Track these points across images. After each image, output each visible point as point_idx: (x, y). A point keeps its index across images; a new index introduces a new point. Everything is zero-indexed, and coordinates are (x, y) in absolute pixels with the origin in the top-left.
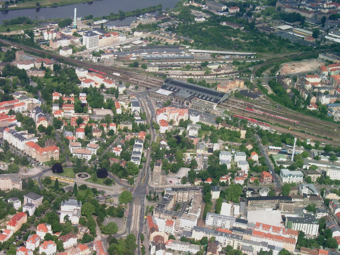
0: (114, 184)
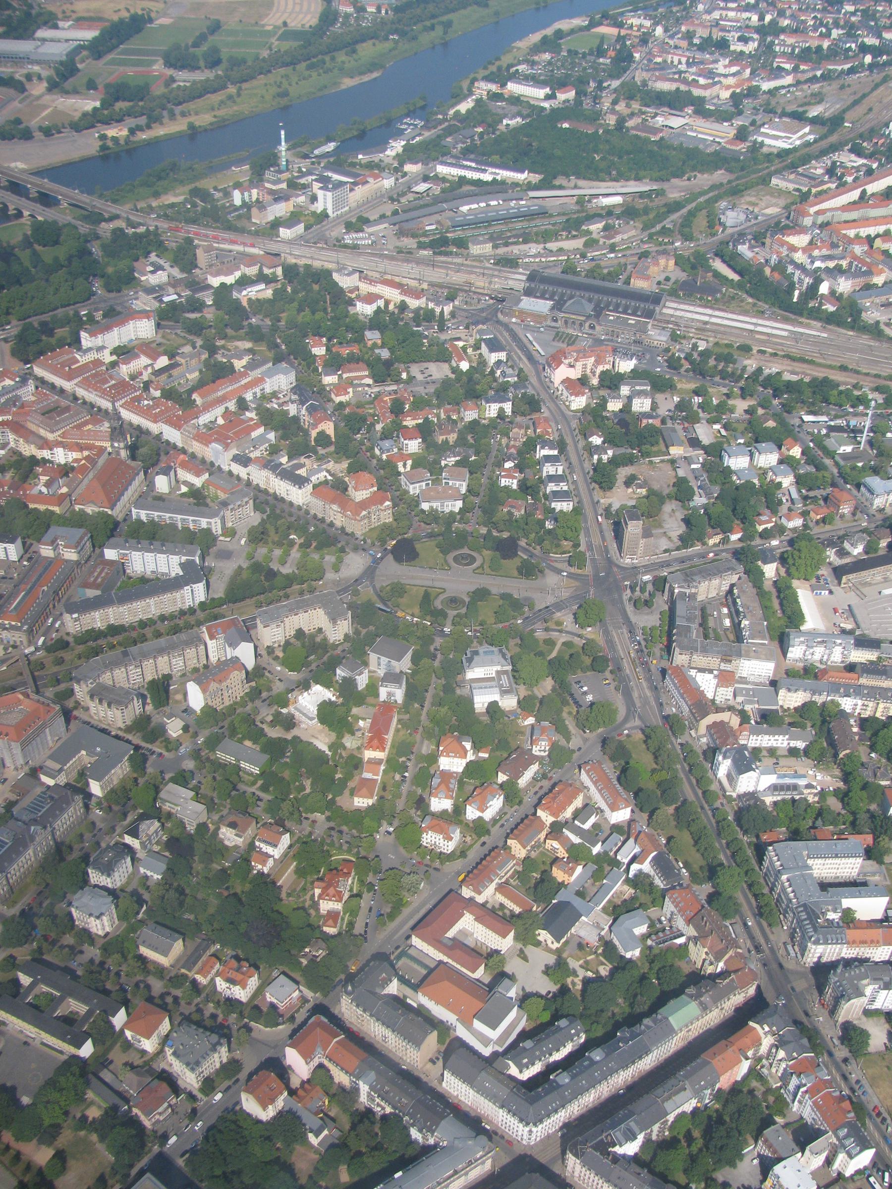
0: (541, 572)
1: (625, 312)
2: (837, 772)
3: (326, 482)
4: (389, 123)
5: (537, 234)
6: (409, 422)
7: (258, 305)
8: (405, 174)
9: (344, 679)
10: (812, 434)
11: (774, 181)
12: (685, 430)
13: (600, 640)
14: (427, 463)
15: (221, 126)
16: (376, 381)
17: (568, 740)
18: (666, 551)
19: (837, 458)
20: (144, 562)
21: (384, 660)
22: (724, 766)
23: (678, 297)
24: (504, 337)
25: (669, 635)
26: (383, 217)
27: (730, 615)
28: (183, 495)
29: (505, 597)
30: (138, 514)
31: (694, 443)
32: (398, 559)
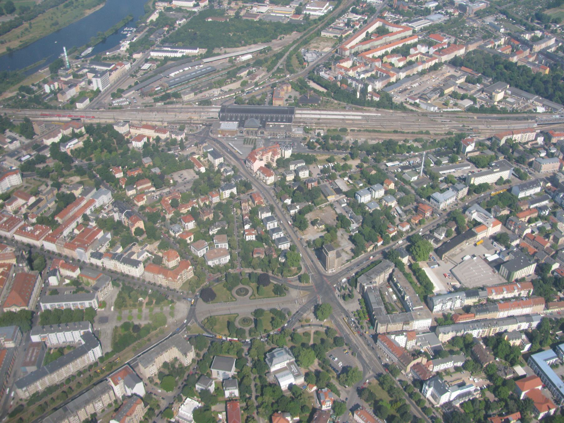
1: (277, 121)
2: (483, 375)
3: (149, 259)
4: (117, 32)
5: (215, 83)
6: (184, 211)
7: (77, 152)
8: (135, 60)
9: (202, 390)
10: (394, 173)
11: (323, 34)
12: (331, 184)
13: (332, 325)
14: (202, 235)
15: (25, 47)
16: (157, 188)
17: (339, 395)
18: (347, 261)
19: (412, 184)
20: (57, 338)
21: (221, 372)
22: (429, 391)
23: (299, 107)
24: (219, 148)
25: (369, 315)
26: (130, 87)
27: (394, 292)
28: (67, 285)
29: (273, 311)
30: (45, 306)
31: (338, 191)
32: (206, 300)
